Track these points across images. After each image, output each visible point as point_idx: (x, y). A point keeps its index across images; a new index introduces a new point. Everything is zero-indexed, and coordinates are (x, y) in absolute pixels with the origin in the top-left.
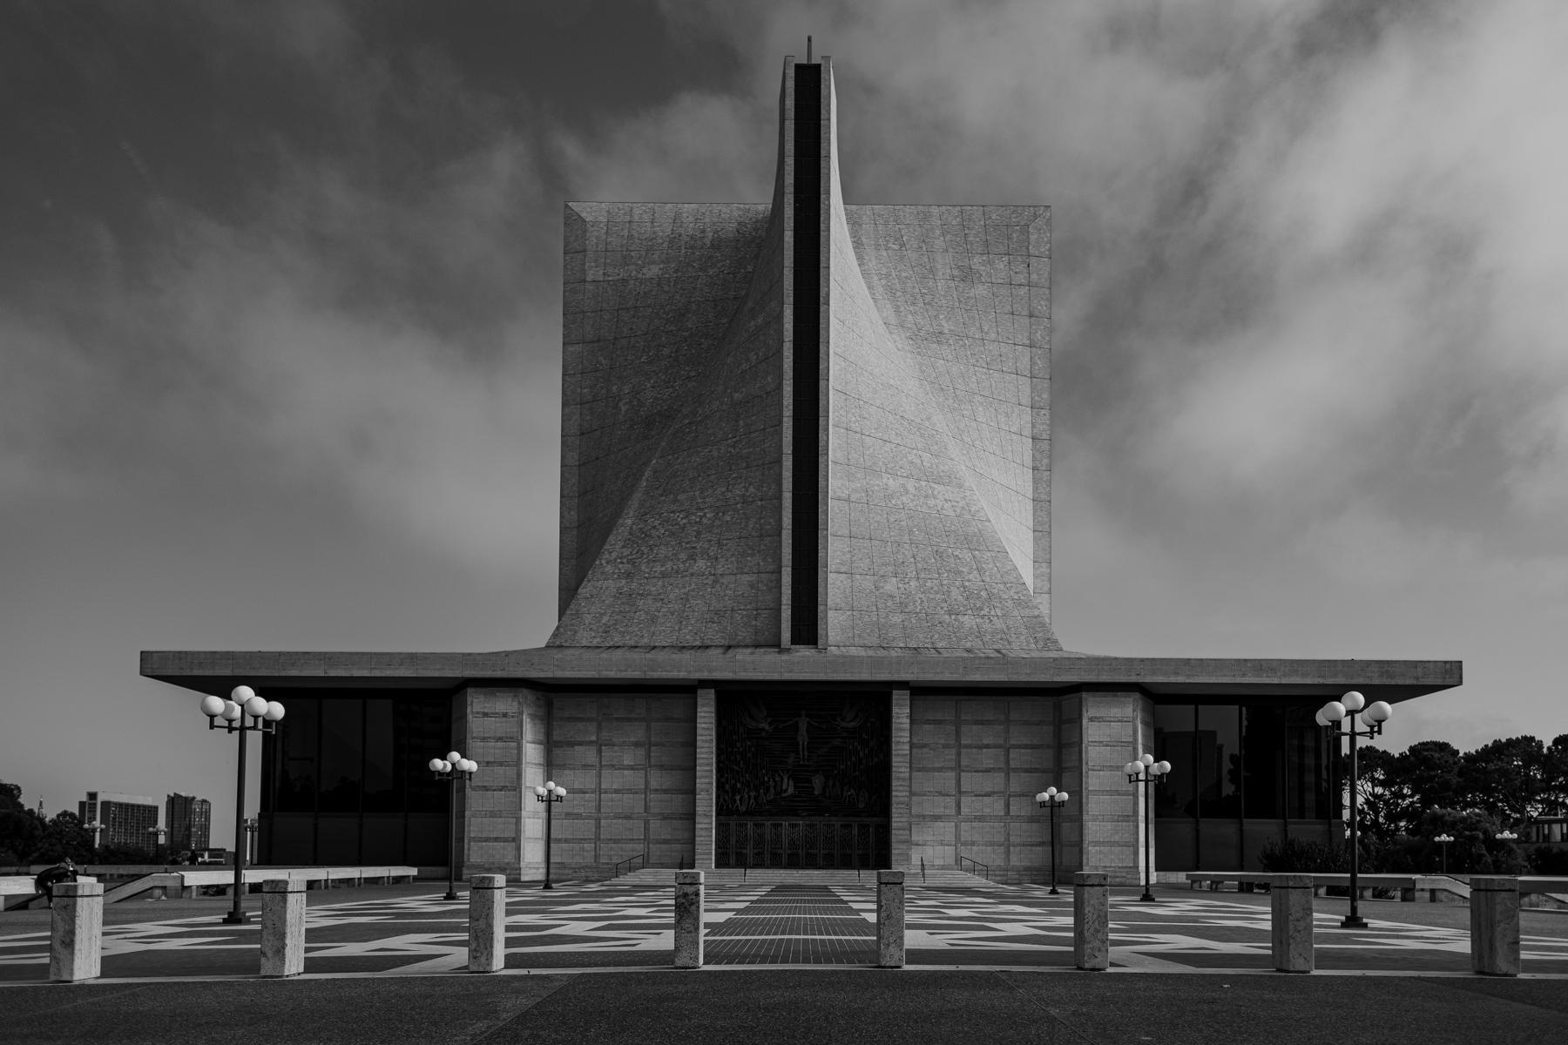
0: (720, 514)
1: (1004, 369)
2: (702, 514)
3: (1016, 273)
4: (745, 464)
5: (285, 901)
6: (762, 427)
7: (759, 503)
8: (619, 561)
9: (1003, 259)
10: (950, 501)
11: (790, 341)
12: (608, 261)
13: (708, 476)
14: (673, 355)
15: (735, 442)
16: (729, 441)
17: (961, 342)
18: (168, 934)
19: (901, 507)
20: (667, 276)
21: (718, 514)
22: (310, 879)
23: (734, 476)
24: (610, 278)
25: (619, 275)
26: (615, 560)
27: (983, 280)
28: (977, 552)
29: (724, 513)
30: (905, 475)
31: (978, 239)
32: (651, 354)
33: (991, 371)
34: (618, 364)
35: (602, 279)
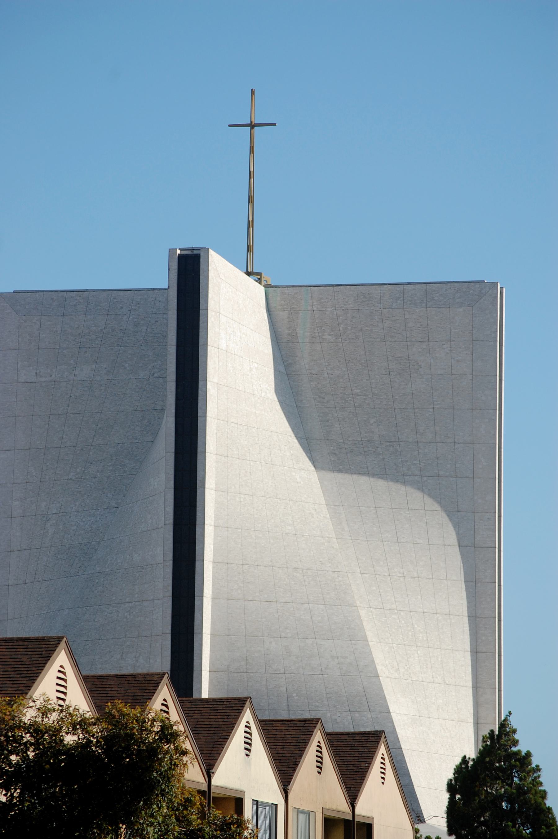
1: (441, 473)
3: (458, 361)
4: (137, 633)
5: (213, 560)
6: (152, 597)
9: (445, 346)
10: (338, 657)
12: (41, 360)
13: (107, 639)
14: (98, 475)
15: (131, 608)
16: (127, 605)
17: (391, 449)
18: (410, 785)
19: (282, 671)
20: (99, 378)
22: (66, 673)
23: (128, 643)
24: (43, 379)
27: (422, 373)
28: (357, 715)
30: (289, 635)
31: (418, 325)
32: (78, 470)
33: (425, 478)
34: (47, 477)
35: (34, 380)
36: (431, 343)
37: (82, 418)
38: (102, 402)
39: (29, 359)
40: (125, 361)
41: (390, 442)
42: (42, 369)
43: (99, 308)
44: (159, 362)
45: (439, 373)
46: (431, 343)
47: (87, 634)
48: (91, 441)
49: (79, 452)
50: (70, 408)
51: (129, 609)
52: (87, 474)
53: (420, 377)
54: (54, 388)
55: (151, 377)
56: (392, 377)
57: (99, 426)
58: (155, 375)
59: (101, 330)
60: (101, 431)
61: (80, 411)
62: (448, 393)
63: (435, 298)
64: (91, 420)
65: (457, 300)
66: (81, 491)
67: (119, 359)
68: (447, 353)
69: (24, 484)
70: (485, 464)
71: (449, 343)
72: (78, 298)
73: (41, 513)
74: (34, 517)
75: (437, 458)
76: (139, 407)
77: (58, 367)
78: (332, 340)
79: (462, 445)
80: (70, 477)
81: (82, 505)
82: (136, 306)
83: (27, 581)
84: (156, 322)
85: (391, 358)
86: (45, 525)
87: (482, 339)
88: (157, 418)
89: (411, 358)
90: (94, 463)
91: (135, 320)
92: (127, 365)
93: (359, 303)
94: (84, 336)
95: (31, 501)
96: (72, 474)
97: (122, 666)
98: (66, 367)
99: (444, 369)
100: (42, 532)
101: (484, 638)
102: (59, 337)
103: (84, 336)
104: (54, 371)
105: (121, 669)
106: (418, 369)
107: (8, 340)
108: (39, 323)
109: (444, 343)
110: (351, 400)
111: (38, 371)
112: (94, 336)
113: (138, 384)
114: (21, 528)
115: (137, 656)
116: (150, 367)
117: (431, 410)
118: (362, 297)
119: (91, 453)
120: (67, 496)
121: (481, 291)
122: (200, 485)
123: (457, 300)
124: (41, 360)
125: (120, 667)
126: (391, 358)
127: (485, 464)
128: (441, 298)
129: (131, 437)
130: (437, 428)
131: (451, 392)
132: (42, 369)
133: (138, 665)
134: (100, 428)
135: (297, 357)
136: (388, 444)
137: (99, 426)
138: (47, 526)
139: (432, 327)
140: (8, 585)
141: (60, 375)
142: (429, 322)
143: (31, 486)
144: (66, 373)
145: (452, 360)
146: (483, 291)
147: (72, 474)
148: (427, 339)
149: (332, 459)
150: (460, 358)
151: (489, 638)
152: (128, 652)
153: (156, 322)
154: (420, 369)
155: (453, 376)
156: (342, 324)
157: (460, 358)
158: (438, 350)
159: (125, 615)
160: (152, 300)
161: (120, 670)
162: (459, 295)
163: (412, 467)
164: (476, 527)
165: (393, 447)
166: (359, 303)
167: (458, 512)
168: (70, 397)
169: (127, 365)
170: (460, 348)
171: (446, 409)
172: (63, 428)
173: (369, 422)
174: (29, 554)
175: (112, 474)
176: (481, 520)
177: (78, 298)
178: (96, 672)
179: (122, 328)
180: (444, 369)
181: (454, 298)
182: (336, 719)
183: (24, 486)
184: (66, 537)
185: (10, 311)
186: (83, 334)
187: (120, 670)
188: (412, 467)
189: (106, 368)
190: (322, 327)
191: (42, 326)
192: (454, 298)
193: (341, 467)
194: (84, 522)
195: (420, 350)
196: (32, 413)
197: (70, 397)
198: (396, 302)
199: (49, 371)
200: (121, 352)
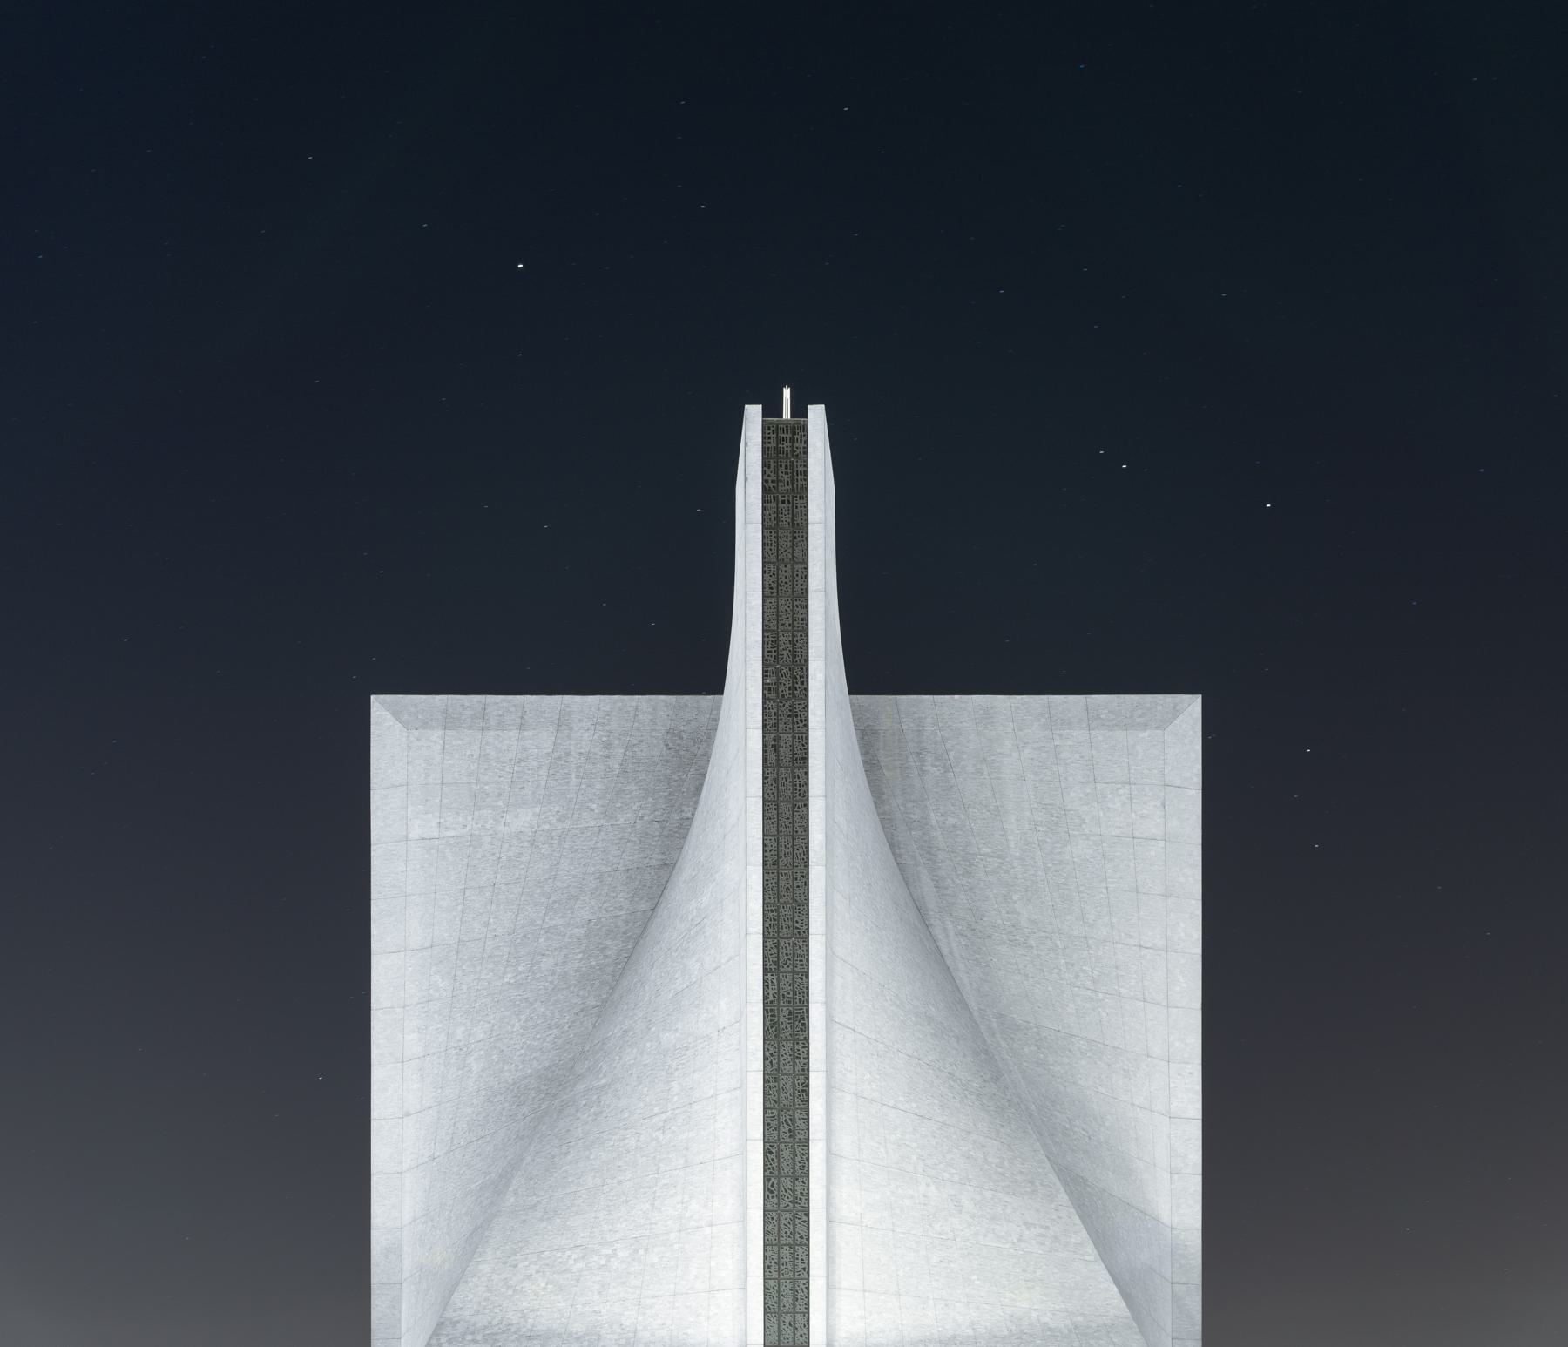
0: (641, 1252)
2: (610, 1252)
7: (708, 1230)
8: (469, 1337)
9: (1121, 792)
11: (756, 933)
12: (446, 801)
15: (665, 1121)
16: (655, 1119)
21: (636, 1251)
23: (664, 1181)
24: (450, 833)
25: (465, 826)
26: (463, 1336)
27: (1087, 831)
29: (647, 1250)
31: (1077, 756)
32: (520, 969)
34: (465, 987)
35: (436, 834)
36: (1099, 787)
37: (521, 889)
38: (555, 862)
39: (427, 800)
40: (591, 800)
41: (1044, 932)
42: (450, 816)
43: (543, 720)
44: (650, 799)
45: (1114, 833)
46: (1099, 787)
47: (576, 1181)
48: (539, 922)
49: (519, 941)
50: (499, 876)
51: (661, 1124)
52: (536, 971)
53: (1084, 837)
54: (470, 846)
55: (638, 821)
56: (1039, 834)
57: (553, 898)
58: (645, 818)
59: (548, 753)
60: (556, 905)
61: (517, 879)
62: (1129, 866)
63: (1102, 717)
64: (539, 891)
65: (1138, 720)
66: (527, 998)
67: (580, 797)
68: (1125, 803)
69: (423, 1005)
70: (1185, 985)
71: (1127, 787)
72: (505, 704)
73: (456, 1045)
74: (443, 1054)
75: (1117, 967)
76: (621, 865)
77: (476, 813)
78: (938, 773)
79: (1151, 951)
80: (506, 980)
81: (532, 1018)
82: (604, 718)
83: (437, 1154)
84: (641, 741)
85: (1036, 805)
86: (465, 1061)
87: (1178, 784)
88: (655, 877)
89: (1069, 808)
90: (547, 953)
91: (604, 739)
92: (594, 806)
93: (977, 721)
94: (519, 762)
95: (438, 1029)
96: (509, 975)
97: (653, 1221)
98: (490, 811)
99: (1120, 828)
100: (460, 1072)
101: (1183, 1262)
102: (476, 766)
103: (519, 762)
104: (470, 818)
105: (654, 1226)
106: (1080, 825)
107: (390, 771)
108: (441, 742)
109: (1120, 786)
110: (978, 862)
111: (442, 820)
112: (535, 764)
113: (617, 833)
114: (421, 1075)
115: (685, 1200)
116: (635, 808)
117: (1105, 891)
118: (981, 712)
119: (541, 940)
120: (502, 1009)
121: (1175, 708)
122: (815, 860)
123: (1138, 720)
124: (446, 801)
125: (651, 1224)
126: (1036, 805)
127: (1185, 985)
128: (1112, 716)
129: (611, 908)
130: (1114, 920)
131: (1132, 865)
132: (450, 816)
133: (687, 1215)
134: (554, 902)
135: (884, 794)
136: (1043, 934)
137: (553, 898)
138: (468, 1062)
139: (1098, 761)
140: (400, 1171)
141: (479, 826)
142: (1094, 752)
143: (436, 1005)
144: (491, 822)
145: (1133, 814)
146: (1178, 708)
147: (509, 975)
148: (1091, 779)
149: (963, 943)
150: (1145, 812)
151: (1191, 1262)
152: (666, 1195)
153: (641, 741)
154: (1084, 826)
155: (1135, 840)
156: (952, 750)
157: (1145, 812)
158: (1110, 796)
159: (654, 1136)
160: (632, 709)
161: (651, 1229)
162: (1140, 712)
163: (1082, 975)
164: (1172, 1085)
165: (1051, 940)
166: (977, 721)
167: (1148, 1056)
168: (499, 858)
169: (594, 806)
170: (1145, 795)
171: (1125, 891)
172: (489, 907)
173: (1011, 899)
174: (438, 1112)
175: (584, 964)
176: (1179, 1075)
177: (505, 704)
178: (602, 1238)
179: (582, 751)
180: (1120, 828)
181: (1131, 717)
182: (1047, 1323)
183: (423, 1008)
184: (506, 1068)
185: (392, 723)
186: (517, 760)
187: (651, 1229)
188: (1082, 975)
189: (558, 812)
190: (921, 753)
191: (446, 746)
192: (1131, 717)
193: (978, 956)
194: (539, 1039)
195: (1082, 795)
196: (433, 888)
197: (499, 858)
198: (1039, 721)
199: (460, 819)
200: (583, 786)
